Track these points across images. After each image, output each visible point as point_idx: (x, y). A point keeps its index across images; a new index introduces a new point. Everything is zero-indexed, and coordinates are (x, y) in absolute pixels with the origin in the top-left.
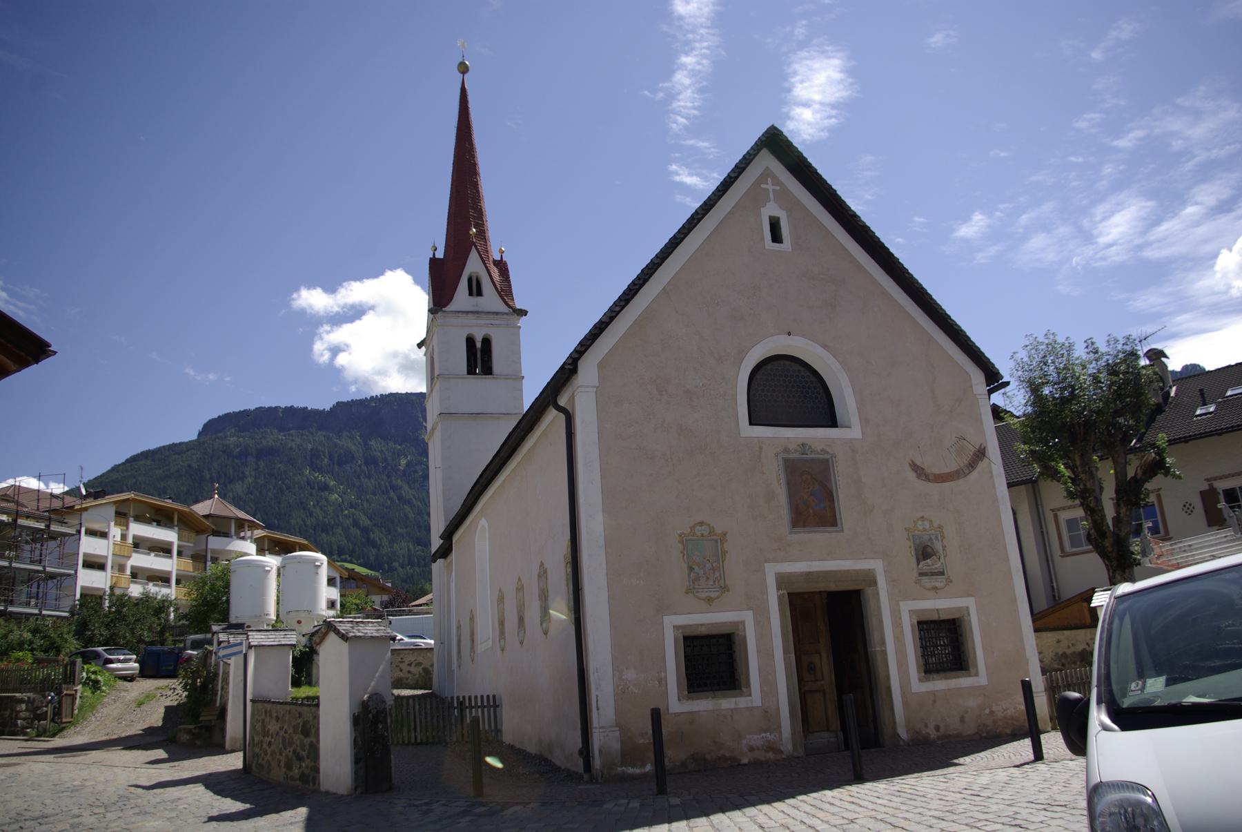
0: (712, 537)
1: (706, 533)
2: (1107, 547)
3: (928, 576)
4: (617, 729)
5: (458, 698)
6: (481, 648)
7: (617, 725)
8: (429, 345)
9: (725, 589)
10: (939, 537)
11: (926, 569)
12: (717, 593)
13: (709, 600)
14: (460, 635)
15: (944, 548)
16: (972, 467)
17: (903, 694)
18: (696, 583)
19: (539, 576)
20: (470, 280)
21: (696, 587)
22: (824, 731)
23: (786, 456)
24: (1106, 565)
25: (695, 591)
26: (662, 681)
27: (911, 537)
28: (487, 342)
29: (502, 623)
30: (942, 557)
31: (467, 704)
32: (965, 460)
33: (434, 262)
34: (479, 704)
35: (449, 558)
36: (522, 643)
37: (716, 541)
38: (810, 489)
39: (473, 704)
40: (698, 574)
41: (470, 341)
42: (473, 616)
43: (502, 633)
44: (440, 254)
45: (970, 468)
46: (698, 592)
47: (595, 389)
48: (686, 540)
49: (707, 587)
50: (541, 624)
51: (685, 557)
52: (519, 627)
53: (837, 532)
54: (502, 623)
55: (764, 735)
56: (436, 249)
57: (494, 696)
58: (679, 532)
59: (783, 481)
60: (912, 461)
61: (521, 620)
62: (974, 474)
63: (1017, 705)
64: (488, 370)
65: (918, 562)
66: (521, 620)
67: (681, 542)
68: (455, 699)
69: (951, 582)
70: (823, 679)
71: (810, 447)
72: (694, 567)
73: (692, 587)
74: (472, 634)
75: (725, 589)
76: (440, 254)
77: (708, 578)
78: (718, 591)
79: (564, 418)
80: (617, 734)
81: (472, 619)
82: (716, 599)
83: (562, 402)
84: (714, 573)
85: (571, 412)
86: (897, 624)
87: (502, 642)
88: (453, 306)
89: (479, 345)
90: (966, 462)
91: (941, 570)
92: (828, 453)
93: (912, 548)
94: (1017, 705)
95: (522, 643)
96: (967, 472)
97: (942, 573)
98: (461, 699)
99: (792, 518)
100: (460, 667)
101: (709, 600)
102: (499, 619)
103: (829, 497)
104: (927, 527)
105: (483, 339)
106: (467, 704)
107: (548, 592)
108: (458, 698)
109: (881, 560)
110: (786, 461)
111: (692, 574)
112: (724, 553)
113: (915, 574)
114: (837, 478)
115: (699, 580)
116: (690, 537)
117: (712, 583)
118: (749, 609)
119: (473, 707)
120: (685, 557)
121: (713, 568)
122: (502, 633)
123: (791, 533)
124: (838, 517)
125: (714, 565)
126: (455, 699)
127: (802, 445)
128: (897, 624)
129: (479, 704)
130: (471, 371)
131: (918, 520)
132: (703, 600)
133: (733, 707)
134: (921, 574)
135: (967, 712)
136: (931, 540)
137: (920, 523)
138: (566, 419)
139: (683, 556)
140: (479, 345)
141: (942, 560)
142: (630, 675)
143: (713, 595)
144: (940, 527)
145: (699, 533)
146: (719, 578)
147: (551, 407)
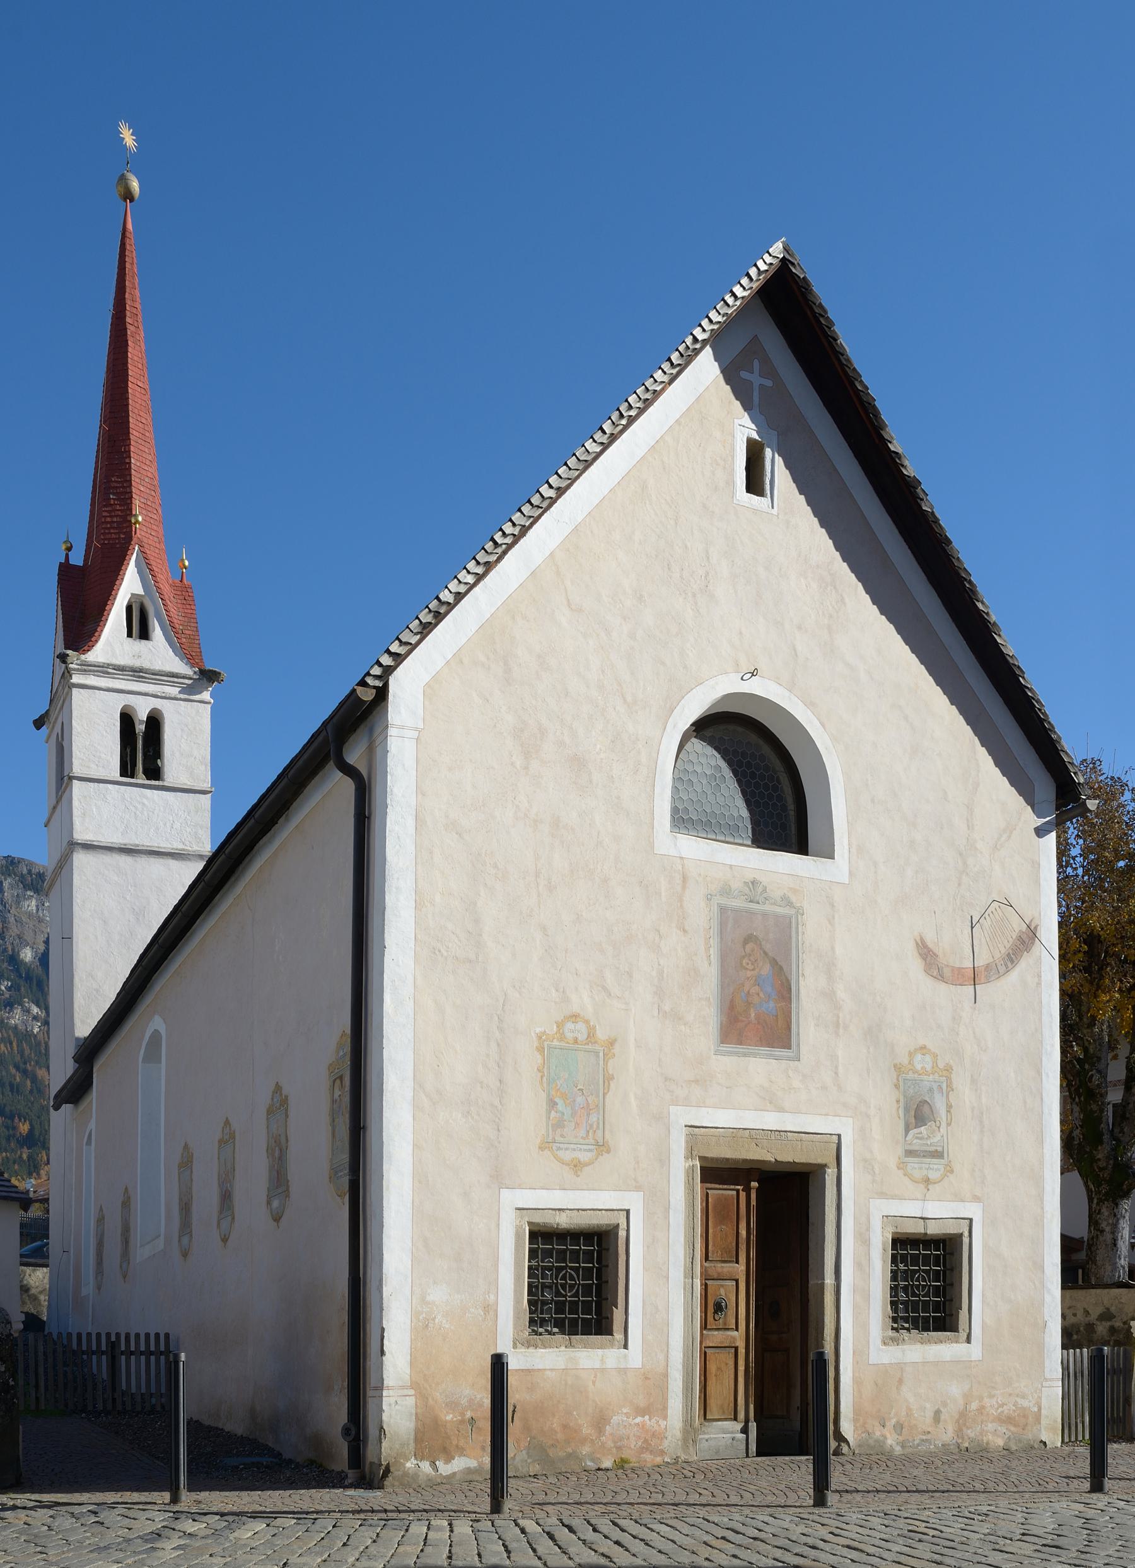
0: (590, 1047)
1: (582, 1037)
2: (1099, 1160)
3: (918, 1156)
4: (412, 1392)
5: (108, 1335)
6: (141, 1253)
7: (414, 1385)
8: (55, 722)
9: (602, 1147)
10: (944, 1086)
11: (917, 1145)
12: (589, 1154)
13: (575, 1166)
14: (102, 1235)
15: (949, 1107)
16: (1012, 961)
17: (856, 1363)
18: (559, 1131)
19: (270, 1112)
20: (129, 609)
21: (558, 1138)
22: (726, 1420)
23: (724, 901)
24: (1089, 1190)
25: (555, 1146)
26: (490, 1310)
27: (901, 1083)
28: (154, 722)
29: (186, 1208)
30: (944, 1124)
31: (123, 1348)
32: (1004, 946)
33: (66, 571)
34: (143, 1348)
35: (84, 1105)
36: (225, 1240)
37: (597, 1053)
38: (755, 972)
39: (133, 1349)
40: (563, 1114)
41: (127, 720)
42: (129, 1198)
43: (186, 1225)
44: (77, 559)
45: (1009, 964)
46: (559, 1149)
47: (416, 734)
48: (550, 1047)
49: (575, 1141)
50: (269, 1203)
51: (545, 1079)
52: (221, 1212)
53: (789, 1059)
54: (186, 1208)
55: (639, 1420)
56: (69, 549)
57: (167, 1336)
58: (538, 1030)
59: (714, 952)
60: (922, 939)
61: (226, 1197)
62: (1014, 976)
63: (1019, 1400)
64: (154, 772)
65: (907, 1130)
66: (226, 1197)
67: (541, 1049)
68: (94, 1337)
69: (952, 1172)
70: (737, 1329)
71: (765, 890)
72: (557, 1100)
73: (550, 1139)
74: (126, 1230)
75: (602, 1147)
76: (77, 559)
77: (577, 1125)
78: (590, 1150)
79: (353, 787)
80: (411, 1401)
81: (126, 1204)
82: (587, 1164)
83: (354, 756)
84: (588, 1115)
85: (364, 773)
86: (863, 1239)
87: (185, 1240)
88: (98, 653)
89: (140, 728)
90: (1003, 951)
91: (939, 1149)
92: (790, 904)
93: (902, 1104)
94: (1019, 1400)
95: (225, 1240)
96: (1002, 969)
97: (937, 1155)
98: (113, 1339)
99: (721, 1024)
100: (99, 1289)
101: (577, 1166)
102: (181, 1199)
103: (785, 991)
104: (929, 1068)
105: (148, 718)
106: (123, 1348)
107: (287, 1140)
108: (108, 1335)
109: (851, 1120)
110: (723, 910)
111: (553, 1114)
112: (608, 1079)
113: (900, 1151)
114: (800, 954)
115: (563, 1127)
116: (556, 1043)
117: (582, 1133)
118: (638, 1188)
119: (132, 1353)
120: (545, 1079)
121: (588, 1104)
122: (186, 1225)
123: (717, 1053)
124: (794, 1026)
125: (589, 1099)
126: (94, 1337)
127: (753, 883)
128: (863, 1239)
129: (143, 1348)
130: (127, 769)
131: (916, 1050)
132: (568, 1165)
133: (597, 1365)
134: (910, 1153)
135: (945, 1404)
136: (931, 1090)
137: (919, 1057)
138: (356, 789)
139: (542, 1077)
140: (140, 728)
141: (943, 1130)
142: (438, 1295)
143: (584, 1157)
144: (948, 1069)
145: (570, 1036)
146: (595, 1126)
147: (331, 765)
